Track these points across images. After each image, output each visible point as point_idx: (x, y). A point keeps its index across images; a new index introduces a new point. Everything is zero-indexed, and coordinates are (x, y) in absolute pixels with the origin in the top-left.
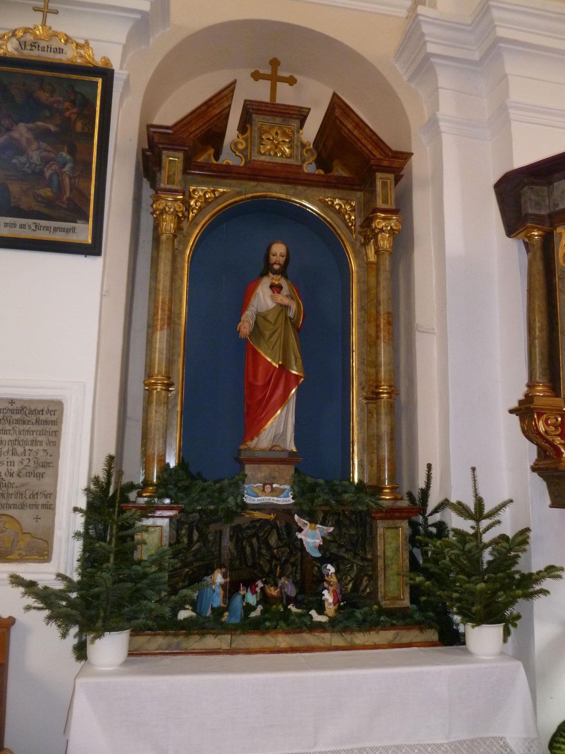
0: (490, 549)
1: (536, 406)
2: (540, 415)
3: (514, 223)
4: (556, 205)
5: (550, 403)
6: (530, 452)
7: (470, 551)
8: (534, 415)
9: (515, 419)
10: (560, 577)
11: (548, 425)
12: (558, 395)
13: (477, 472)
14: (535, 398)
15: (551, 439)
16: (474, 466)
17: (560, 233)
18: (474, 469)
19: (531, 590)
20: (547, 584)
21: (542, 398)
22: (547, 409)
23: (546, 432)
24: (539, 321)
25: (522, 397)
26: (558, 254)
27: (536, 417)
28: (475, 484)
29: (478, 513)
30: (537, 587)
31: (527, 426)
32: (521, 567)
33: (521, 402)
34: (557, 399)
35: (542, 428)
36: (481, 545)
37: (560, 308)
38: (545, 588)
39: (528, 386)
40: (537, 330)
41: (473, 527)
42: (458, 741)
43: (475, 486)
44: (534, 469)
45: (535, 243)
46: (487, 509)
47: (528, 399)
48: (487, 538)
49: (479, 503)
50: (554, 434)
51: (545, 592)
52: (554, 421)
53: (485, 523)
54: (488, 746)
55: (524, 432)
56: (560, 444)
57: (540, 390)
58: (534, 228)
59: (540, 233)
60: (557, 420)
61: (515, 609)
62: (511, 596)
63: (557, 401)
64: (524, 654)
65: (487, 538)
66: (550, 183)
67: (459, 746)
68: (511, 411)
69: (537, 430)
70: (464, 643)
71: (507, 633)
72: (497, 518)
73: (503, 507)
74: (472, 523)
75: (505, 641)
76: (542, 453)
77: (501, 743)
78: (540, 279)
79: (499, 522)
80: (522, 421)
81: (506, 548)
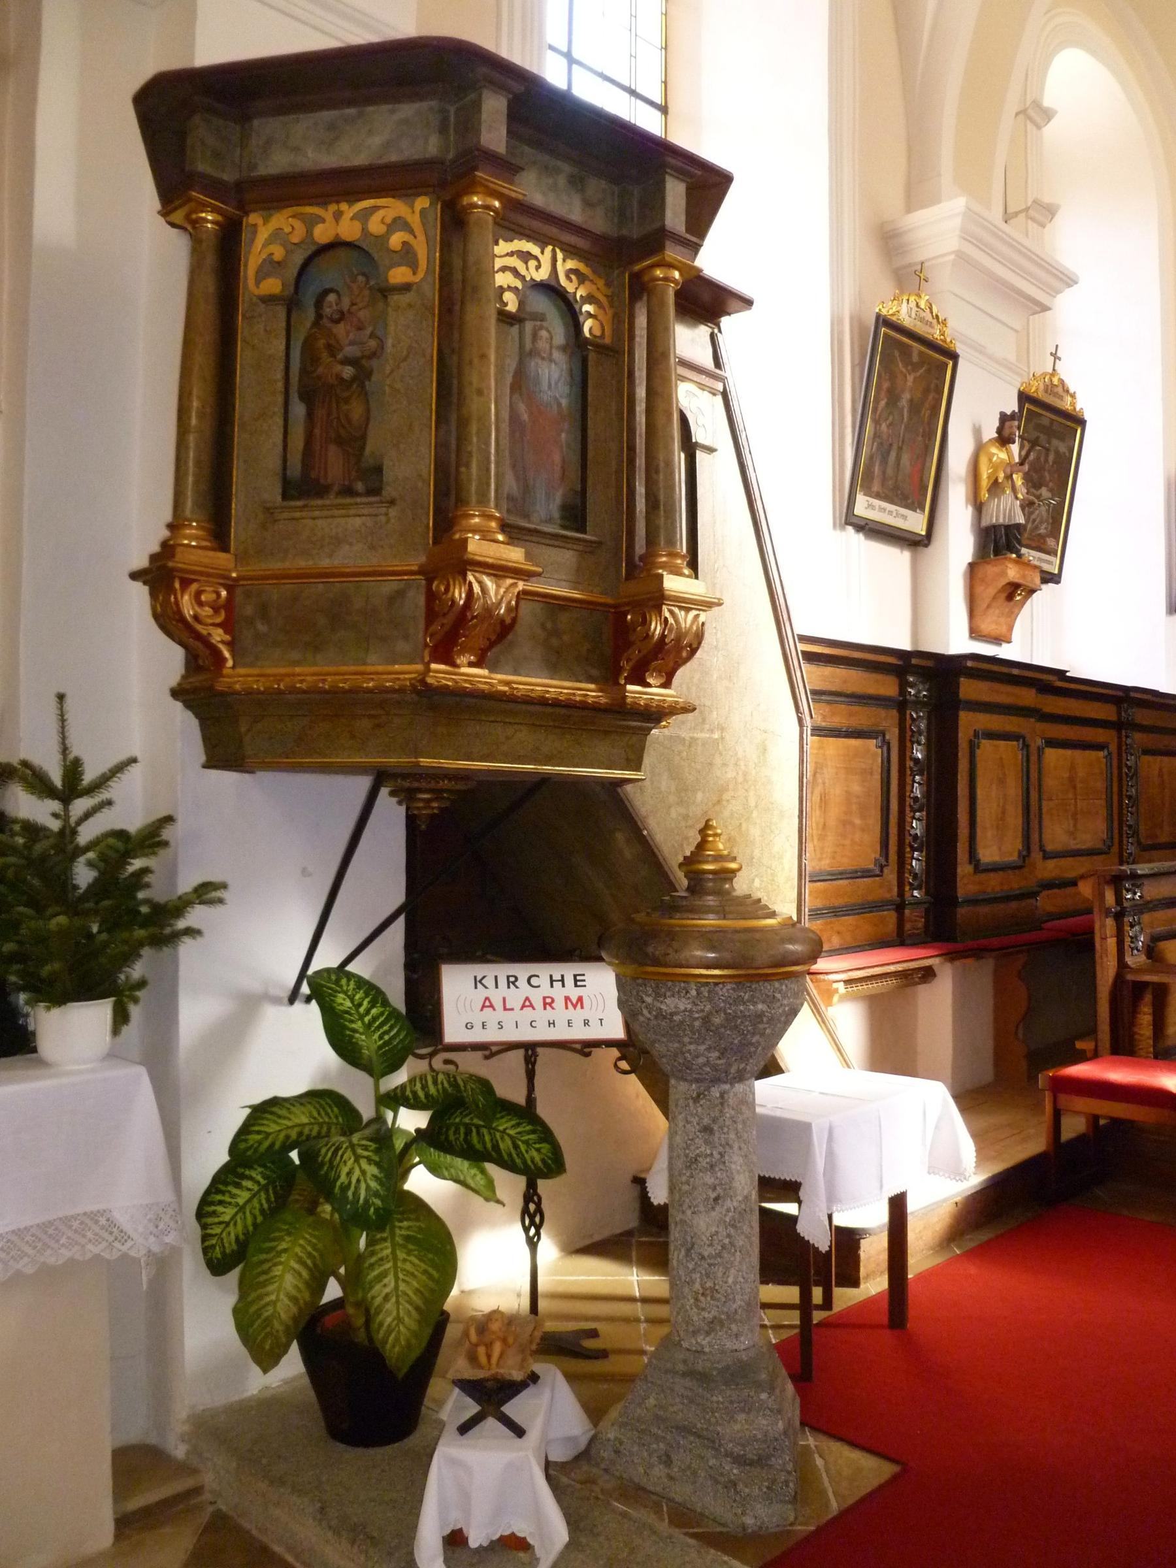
0: (91, 855)
1: (180, 565)
2: (185, 583)
3: (175, 187)
4: (254, 167)
5: (206, 561)
6: (171, 660)
7: (44, 858)
8: (173, 583)
9: (140, 592)
10: (221, 901)
11: (201, 604)
12: (225, 549)
13: (69, 703)
14: (179, 549)
15: (204, 632)
16: (62, 691)
17: (255, 225)
18: (61, 697)
19: (168, 930)
20: (196, 916)
21: (193, 550)
22: (201, 573)
23: (196, 618)
24: (198, 397)
25: (156, 548)
26: (246, 265)
27: (177, 585)
28: (63, 727)
29: (73, 785)
30: (181, 924)
31: (161, 606)
32: (156, 891)
33: (153, 558)
34: (222, 555)
35: (188, 608)
36: (70, 847)
37: (241, 377)
38: (196, 926)
39: (171, 527)
40: (194, 414)
41: (55, 815)
42: (13, 1231)
43: (63, 733)
44: (176, 693)
45: (204, 237)
46: (89, 776)
47: (167, 549)
48: (87, 834)
49: (73, 769)
50: (210, 621)
51: (191, 932)
52: (214, 596)
53: (80, 806)
54: (76, 1231)
55: (156, 616)
56: (223, 642)
57: (192, 537)
58: (203, 207)
59: (219, 218)
60: (218, 595)
61: (137, 971)
62: (125, 942)
63: (222, 559)
64: (159, 1058)
65: (87, 834)
66: (245, 119)
67: (14, 1238)
68: (134, 576)
69: (179, 612)
70: (34, 1050)
71: (121, 1018)
72: (104, 795)
73: (117, 772)
74: (55, 805)
75: (116, 1031)
76: (193, 664)
77: (103, 1221)
78: (208, 311)
79: (109, 803)
80: (153, 595)
81: (117, 851)
